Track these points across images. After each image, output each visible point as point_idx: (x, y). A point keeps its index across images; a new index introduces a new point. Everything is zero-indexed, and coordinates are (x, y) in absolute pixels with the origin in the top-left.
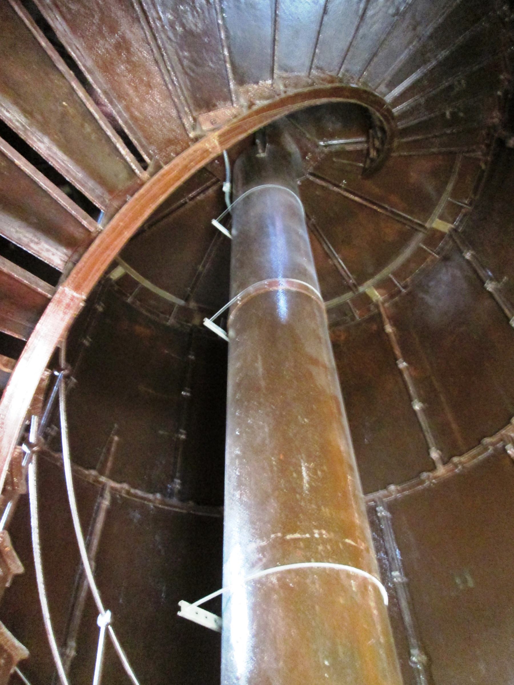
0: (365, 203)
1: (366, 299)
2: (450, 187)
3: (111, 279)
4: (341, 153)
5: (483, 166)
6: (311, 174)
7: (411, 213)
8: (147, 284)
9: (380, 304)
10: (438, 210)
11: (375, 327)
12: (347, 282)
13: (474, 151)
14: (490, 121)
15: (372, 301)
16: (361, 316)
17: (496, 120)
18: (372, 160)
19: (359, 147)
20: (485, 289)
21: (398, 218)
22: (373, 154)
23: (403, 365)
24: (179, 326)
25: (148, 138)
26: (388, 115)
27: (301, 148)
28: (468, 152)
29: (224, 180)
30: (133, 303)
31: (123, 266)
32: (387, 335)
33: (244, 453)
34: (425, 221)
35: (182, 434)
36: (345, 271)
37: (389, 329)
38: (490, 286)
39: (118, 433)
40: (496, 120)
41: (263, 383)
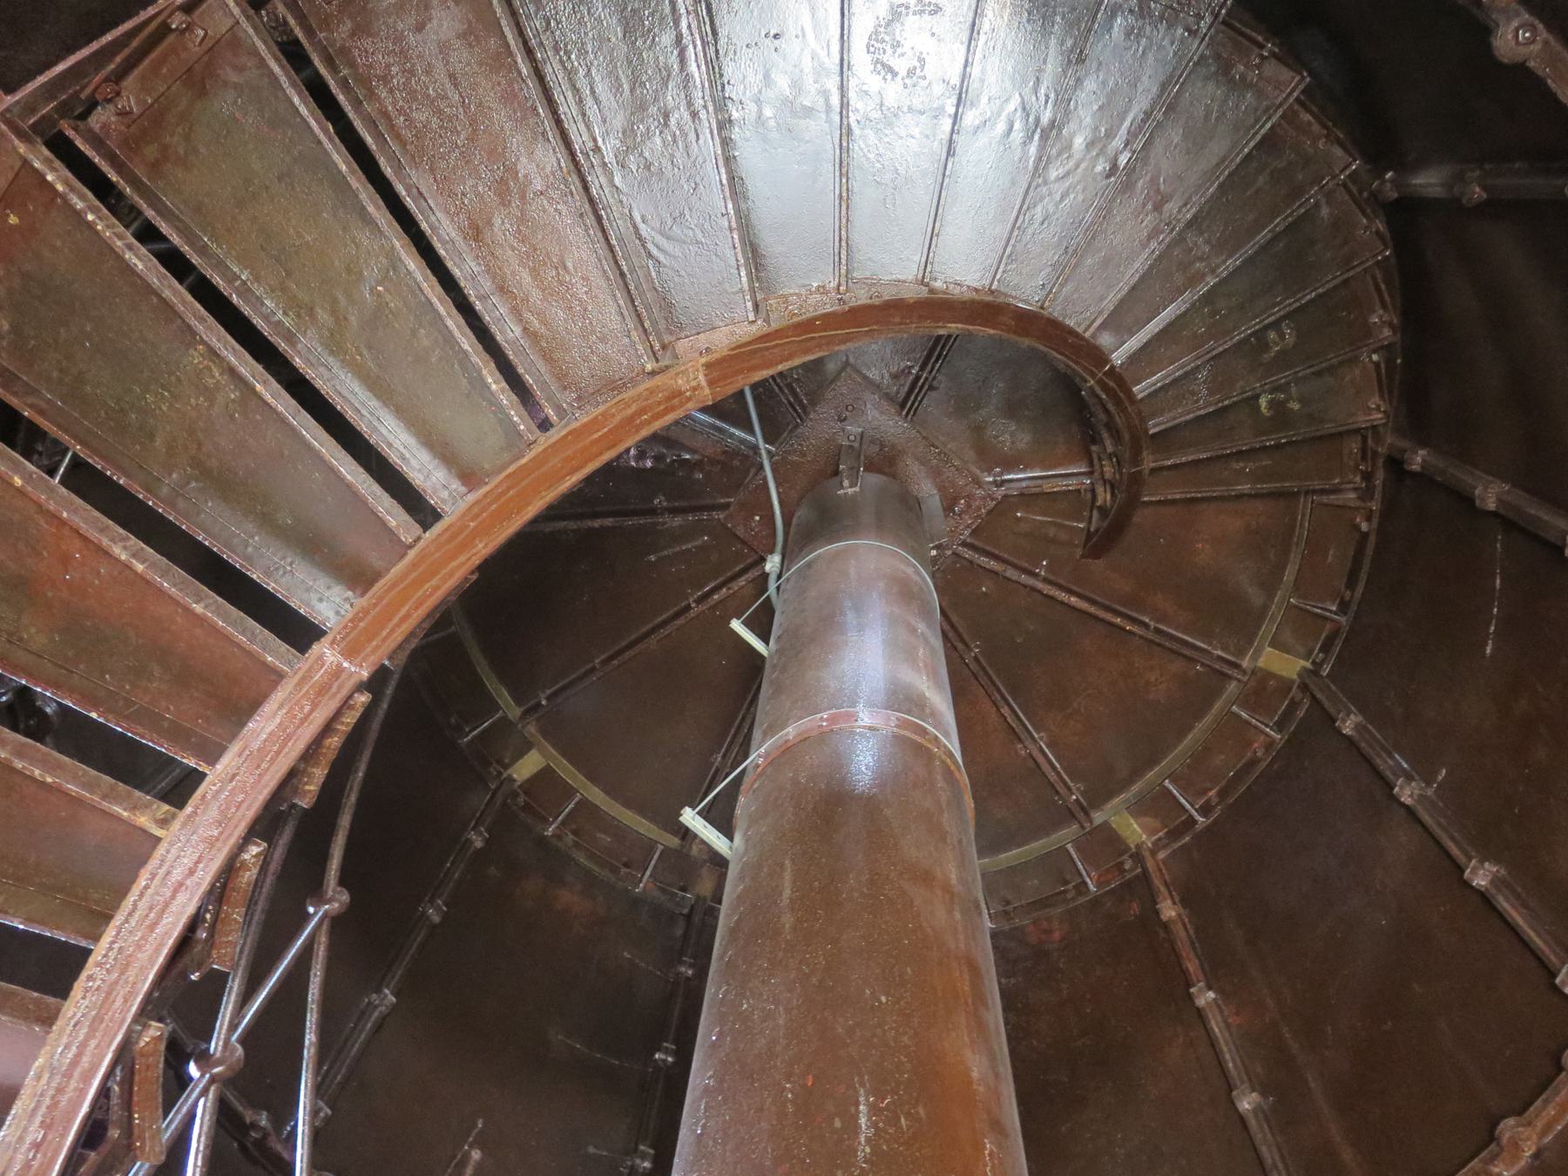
0: (1092, 609)
1: (1106, 842)
2: (1289, 575)
3: (511, 780)
4: (1028, 498)
5: (1364, 527)
6: (964, 544)
7: (1206, 635)
8: (596, 796)
9: (1147, 854)
10: (1268, 629)
11: (1135, 908)
12: (1064, 801)
13: (1336, 490)
14: (1362, 420)
15: (1128, 848)
16: (1099, 885)
17: (1377, 417)
18: (1103, 511)
19: (1072, 484)
20: (1395, 799)
21: (1175, 646)
22: (1104, 496)
23: (1205, 997)
24: (657, 893)
25: (562, 377)
26: (1118, 382)
27: (942, 489)
28: (1323, 492)
29: (772, 552)
30: (558, 837)
31: (542, 752)
32: (1165, 926)
33: (721, 1081)
34: (1241, 653)
35: (643, 1157)
36: (1058, 774)
37: (1169, 910)
38: (1407, 793)
39: (480, 1143)
40: (1377, 417)
41: (788, 921)
